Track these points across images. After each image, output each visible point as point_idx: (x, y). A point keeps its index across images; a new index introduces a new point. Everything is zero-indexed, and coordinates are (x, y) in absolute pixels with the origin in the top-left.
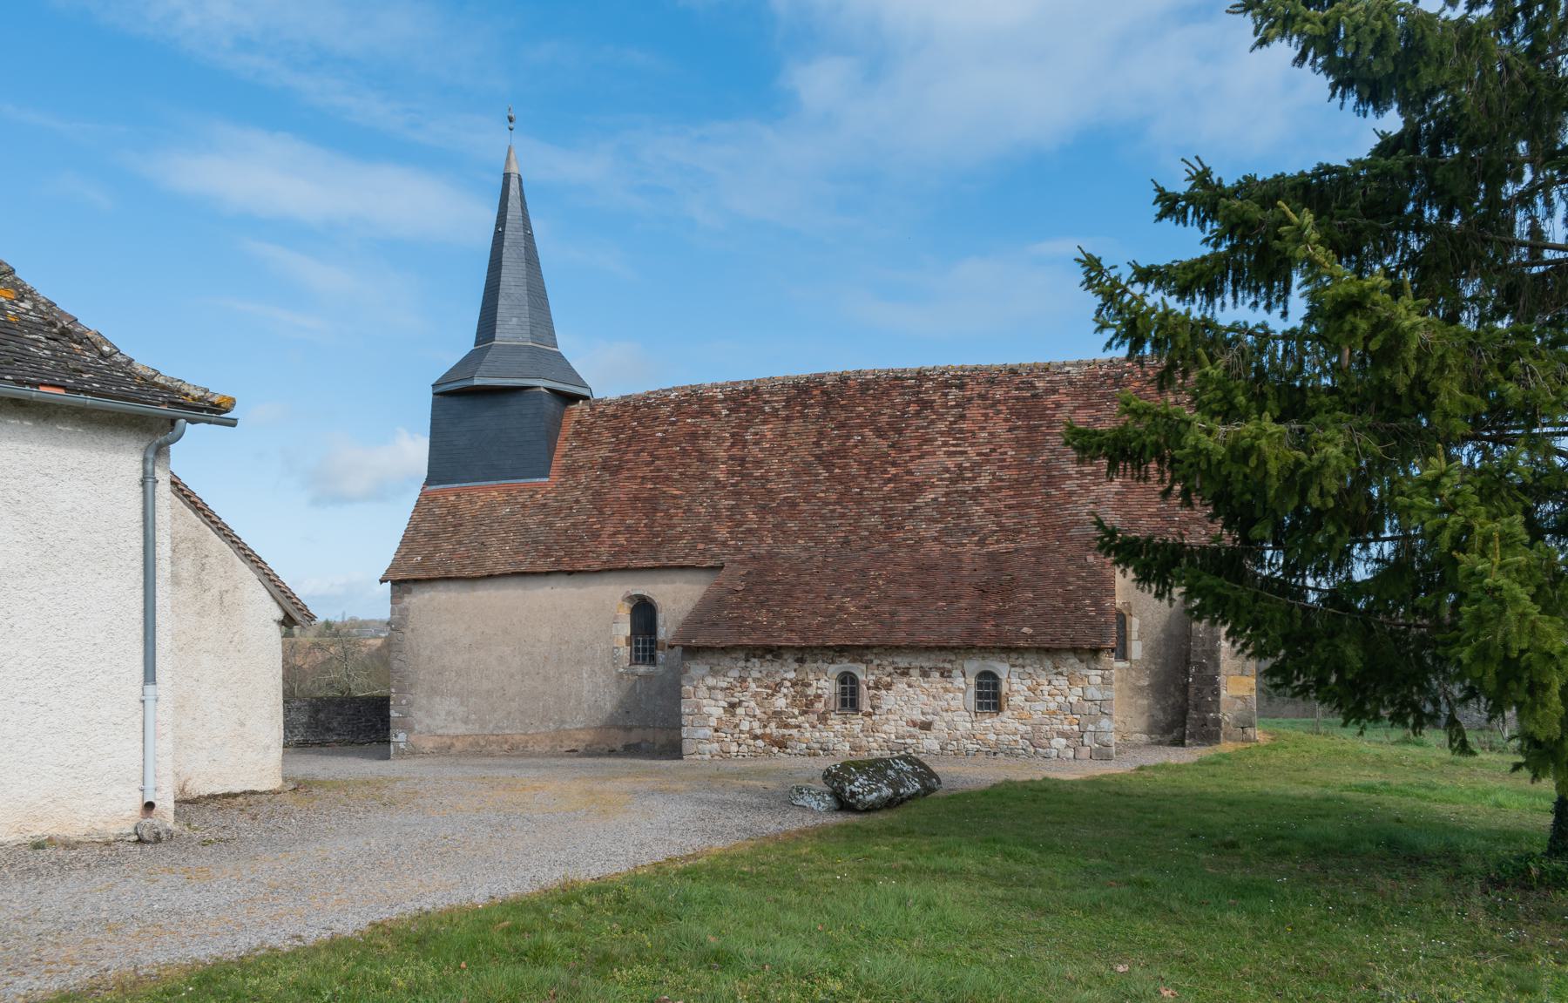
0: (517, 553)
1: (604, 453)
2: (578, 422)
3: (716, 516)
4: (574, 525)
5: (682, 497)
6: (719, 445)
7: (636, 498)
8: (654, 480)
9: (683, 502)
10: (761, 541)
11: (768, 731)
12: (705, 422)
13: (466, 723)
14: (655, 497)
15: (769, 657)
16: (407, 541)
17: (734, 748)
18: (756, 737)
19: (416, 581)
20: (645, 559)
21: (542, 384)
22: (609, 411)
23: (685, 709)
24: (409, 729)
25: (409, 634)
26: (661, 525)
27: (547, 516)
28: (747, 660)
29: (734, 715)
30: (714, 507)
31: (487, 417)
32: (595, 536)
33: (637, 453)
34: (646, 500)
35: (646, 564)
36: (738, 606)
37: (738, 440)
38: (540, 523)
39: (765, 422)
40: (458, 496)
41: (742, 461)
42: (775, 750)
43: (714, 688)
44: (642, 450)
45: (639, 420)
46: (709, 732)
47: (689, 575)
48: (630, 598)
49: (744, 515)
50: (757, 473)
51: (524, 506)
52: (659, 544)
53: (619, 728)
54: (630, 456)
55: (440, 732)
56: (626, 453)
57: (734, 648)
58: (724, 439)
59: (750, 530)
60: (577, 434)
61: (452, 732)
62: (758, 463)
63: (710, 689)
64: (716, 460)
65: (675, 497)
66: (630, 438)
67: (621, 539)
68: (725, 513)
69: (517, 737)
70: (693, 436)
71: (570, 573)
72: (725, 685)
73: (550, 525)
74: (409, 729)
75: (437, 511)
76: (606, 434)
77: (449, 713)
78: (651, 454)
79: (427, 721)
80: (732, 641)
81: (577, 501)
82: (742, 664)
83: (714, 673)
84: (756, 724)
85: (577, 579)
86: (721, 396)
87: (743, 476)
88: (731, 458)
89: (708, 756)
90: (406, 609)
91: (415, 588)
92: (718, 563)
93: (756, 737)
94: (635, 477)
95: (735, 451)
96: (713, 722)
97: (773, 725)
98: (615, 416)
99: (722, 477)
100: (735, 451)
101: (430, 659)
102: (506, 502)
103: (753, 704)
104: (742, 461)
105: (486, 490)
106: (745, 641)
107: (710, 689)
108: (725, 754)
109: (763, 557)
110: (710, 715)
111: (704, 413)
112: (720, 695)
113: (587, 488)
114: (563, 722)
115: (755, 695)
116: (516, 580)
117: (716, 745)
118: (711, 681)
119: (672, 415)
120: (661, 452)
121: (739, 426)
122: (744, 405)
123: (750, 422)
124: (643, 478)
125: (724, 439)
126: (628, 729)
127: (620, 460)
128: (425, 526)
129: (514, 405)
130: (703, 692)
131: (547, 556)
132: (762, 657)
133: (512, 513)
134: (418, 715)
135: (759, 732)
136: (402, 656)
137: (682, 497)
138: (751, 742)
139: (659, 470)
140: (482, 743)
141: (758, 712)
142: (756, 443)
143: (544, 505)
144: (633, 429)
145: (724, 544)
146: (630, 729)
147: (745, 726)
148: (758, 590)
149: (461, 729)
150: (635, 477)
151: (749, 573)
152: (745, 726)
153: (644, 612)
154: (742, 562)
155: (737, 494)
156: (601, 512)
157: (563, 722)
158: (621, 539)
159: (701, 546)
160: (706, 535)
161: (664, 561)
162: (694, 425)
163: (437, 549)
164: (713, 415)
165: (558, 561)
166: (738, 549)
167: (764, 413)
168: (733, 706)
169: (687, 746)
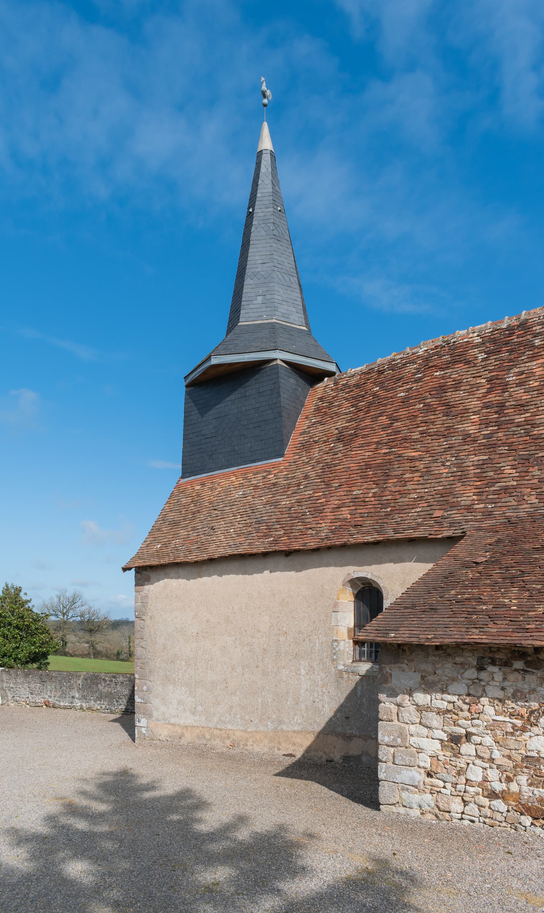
0: (239, 535)
1: (341, 424)
2: (321, 399)
3: (462, 477)
4: (298, 501)
5: (420, 459)
6: (471, 393)
7: (368, 466)
8: (390, 444)
9: (420, 465)
10: (521, 500)
11: (514, 787)
12: (458, 372)
13: (194, 714)
14: (390, 462)
15: (519, 664)
16: (155, 530)
17: (456, 806)
18: (493, 795)
19: (151, 567)
20: (368, 533)
21: (279, 355)
22: (353, 381)
23: (383, 737)
24: (149, 715)
25: (148, 622)
26: (392, 493)
27: (274, 495)
28: (480, 668)
29: (457, 754)
30: (459, 466)
31: (233, 403)
32: (318, 511)
33: (375, 418)
34: (379, 466)
35: (369, 538)
36: (474, 583)
37: (497, 384)
38: (268, 503)
39: (533, 358)
40: (203, 484)
41: (501, 407)
42: (527, 820)
43: (428, 709)
44: (381, 415)
45: (381, 385)
46: (419, 777)
47: (421, 550)
48: (353, 582)
49: (499, 471)
50: (519, 419)
51: (256, 487)
52: (388, 515)
53: (338, 735)
54: (368, 422)
55: (173, 721)
56: (363, 419)
57: (460, 648)
58: (479, 386)
59: (506, 490)
60: (318, 409)
61: (182, 722)
62: (521, 407)
63: (420, 709)
64: (466, 410)
65: (412, 460)
66: (370, 404)
67: (345, 513)
68: (473, 471)
69: (238, 734)
70: (442, 388)
71: (288, 553)
72: (444, 705)
73: (276, 504)
74: (149, 715)
75: (184, 501)
76: (346, 404)
77: (180, 702)
78: (390, 417)
79: (163, 708)
80: (453, 636)
81: (306, 477)
82: (472, 673)
83: (428, 686)
84: (493, 774)
85: (296, 560)
86: (478, 340)
87: (499, 425)
88: (486, 406)
89: (415, 813)
90: (146, 596)
91: (153, 575)
92: (458, 533)
93: (493, 795)
94: (369, 444)
95: (492, 398)
96: (425, 761)
97: (523, 779)
98: (357, 386)
99: (472, 429)
100: (492, 398)
101: (165, 647)
102: (242, 485)
103: (488, 740)
104: (501, 407)
105: (227, 476)
106: (476, 636)
107: (420, 709)
108: (441, 811)
109: (521, 520)
110: (420, 750)
111: (455, 362)
112: (435, 720)
113: (318, 462)
114: (281, 722)
115: (492, 727)
116: (236, 565)
117: (428, 797)
118: (421, 698)
119: (418, 371)
120: (403, 413)
121: (499, 368)
122: (507, 344)
123: (513, 362)
124: (378, 443)
125: (479, 386)
126: (348, 738)
127: (356, 428)
128: (171, 516)
129: (253, 386)
130: (410, 712)
131: (266, 536)
132: (506, 664)
133: (245, 496)
134: (156, 702)
135: (498, 787)
136: (143, 643)
137: (420, 459)
138: (486, 802)
139: (398, 432)
140: (208, 737)
141: (497, 755)
142: (519, 385)
143: (274, 484)
144: (374, 395)
145: (469, 508)
146: (348, 738)
147: (476, 774)
148: (508, 560)
149: (189, 720)
150: (369, 444)
151: (499, 541)
152: (476, 774)
153: (368, 596)
154: (493, 530)
155: (491, 447)
156: (328, 485)
157: (281, 722)
158: (345, 513)
159: (437, 513)
160: (446, 499)
161: (390, 534)
162: (443, 378)
163: (176, 536)
164: (467, 362)
165: (276, 542)
166: (489, 514)
167: (533, 347)
168: (455, 739)
169: (385, 792)
